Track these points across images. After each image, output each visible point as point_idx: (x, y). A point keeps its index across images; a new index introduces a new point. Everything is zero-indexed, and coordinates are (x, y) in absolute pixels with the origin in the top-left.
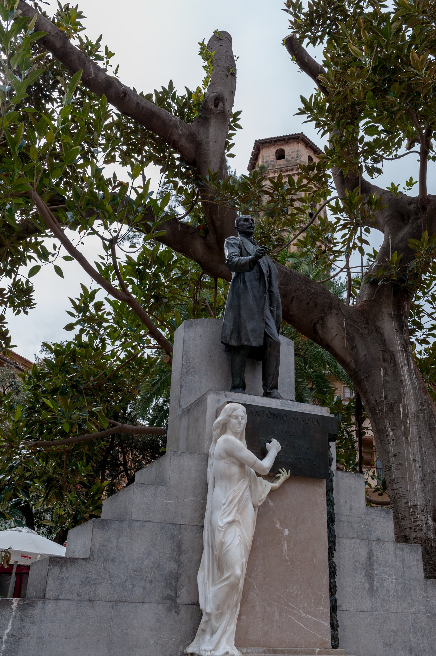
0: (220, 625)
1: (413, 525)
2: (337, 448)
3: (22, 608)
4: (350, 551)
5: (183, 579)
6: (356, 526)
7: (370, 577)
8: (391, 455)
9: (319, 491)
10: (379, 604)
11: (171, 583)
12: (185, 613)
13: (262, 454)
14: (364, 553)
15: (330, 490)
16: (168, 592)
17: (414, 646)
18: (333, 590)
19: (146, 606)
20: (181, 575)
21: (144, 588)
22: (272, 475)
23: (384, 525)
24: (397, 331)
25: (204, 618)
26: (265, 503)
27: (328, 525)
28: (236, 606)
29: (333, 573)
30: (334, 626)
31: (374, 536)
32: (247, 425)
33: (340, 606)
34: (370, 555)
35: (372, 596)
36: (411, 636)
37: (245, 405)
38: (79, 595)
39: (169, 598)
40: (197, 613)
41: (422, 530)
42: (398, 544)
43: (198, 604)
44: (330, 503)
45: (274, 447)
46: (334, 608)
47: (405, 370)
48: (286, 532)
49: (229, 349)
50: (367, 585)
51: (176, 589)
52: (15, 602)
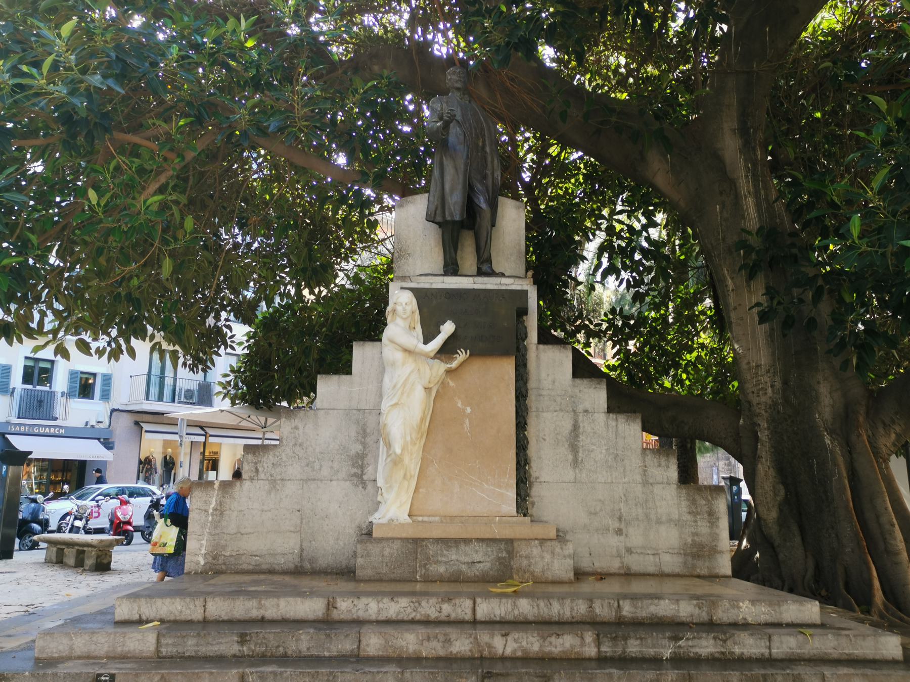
1: (755, 389)
4: (546, 426)
6: (559, 399)
7: (574, 448)
8: (731, 308)
9: (507, 367)
10: (584, 475)
11: (357, 462)
14: (566, 425)
16: (355, 470)
17: (624, 514)
19: (334, 483)
20: (367, 455)
21: (332, 467)
31: (581, 408)
33: (537, 478)
34: (576, 427)
35: (575, 468)
36: (622, 505)
38: (271, 476)
39: (355, 475)
41: (766, 393)
42: (611, 415)
47: (750, 201)
50: (570, 457)
51: (362, 467)
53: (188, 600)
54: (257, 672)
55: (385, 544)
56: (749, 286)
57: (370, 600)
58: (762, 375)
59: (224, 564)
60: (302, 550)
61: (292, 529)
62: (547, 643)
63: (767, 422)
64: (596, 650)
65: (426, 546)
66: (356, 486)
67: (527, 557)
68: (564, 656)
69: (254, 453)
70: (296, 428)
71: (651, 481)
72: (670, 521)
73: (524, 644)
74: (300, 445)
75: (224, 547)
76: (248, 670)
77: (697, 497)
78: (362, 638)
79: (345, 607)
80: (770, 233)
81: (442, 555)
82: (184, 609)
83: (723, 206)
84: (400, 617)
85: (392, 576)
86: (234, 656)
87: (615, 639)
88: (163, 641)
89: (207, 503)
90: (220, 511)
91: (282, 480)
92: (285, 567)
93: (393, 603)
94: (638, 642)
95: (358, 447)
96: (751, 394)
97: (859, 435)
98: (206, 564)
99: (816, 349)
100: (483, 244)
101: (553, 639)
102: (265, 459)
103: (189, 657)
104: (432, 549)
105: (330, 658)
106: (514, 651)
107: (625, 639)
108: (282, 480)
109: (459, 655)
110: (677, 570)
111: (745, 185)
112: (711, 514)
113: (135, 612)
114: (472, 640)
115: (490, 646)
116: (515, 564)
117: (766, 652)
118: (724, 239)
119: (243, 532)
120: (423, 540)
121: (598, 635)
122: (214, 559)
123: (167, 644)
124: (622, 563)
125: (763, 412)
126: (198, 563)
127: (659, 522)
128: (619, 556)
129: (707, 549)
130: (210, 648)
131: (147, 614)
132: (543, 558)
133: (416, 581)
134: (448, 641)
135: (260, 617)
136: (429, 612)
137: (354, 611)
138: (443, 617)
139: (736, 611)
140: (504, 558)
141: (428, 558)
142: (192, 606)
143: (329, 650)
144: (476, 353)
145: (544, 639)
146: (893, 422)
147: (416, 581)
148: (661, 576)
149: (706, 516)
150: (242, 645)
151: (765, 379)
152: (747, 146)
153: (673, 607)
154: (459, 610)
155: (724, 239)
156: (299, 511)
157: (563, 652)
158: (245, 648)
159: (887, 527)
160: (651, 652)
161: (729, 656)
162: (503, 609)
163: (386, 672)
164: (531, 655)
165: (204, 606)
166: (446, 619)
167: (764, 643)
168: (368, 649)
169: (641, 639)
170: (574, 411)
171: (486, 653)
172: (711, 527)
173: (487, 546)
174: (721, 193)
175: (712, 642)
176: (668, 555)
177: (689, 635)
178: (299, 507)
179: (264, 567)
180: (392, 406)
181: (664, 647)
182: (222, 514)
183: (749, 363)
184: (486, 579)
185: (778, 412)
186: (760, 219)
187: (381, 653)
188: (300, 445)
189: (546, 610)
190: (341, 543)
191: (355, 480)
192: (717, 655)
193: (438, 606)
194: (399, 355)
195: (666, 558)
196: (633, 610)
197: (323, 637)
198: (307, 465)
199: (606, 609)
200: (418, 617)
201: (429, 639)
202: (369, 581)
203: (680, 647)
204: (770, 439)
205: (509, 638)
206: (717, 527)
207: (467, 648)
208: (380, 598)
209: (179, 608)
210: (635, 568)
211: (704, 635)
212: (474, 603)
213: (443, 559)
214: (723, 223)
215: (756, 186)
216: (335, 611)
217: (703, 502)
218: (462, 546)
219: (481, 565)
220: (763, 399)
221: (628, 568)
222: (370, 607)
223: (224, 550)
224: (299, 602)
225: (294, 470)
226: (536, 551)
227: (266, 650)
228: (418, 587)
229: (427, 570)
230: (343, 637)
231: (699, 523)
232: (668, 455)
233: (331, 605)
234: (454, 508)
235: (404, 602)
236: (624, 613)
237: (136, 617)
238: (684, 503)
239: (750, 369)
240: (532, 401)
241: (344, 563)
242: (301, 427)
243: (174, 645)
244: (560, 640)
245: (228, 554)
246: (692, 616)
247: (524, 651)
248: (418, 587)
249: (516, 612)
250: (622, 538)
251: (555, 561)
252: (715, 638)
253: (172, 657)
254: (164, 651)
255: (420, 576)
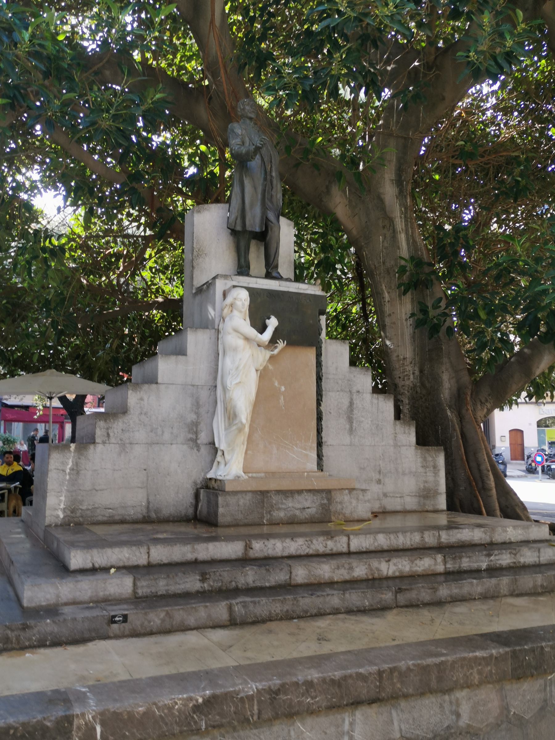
0: (232, 457)
2: (327, 320)
3: (78, 450)
4: (333, 400)
5: (203, 426)
6: (340, 382)
7: (350, 420)
9: (310, 354)
11: (192, 429)
12: (204, 450)
13: (262, 329)
14: (346, 402)
15: (319, 355)
16: (191, 436)
18: (319, 431)
20: (200, 423)
21: (172, 433)
22: (273, 341)
23: (364, 380)
24: (397, 198)
25: (219, 453)
26: (265, 368)
27: (317, 382)
28: (243, 444)
29: (319, 418)
30: (320, 456)
31: (354, 389)
32: (250, 306)
33: (326, 442)
34: (351, 404)
36: (381, 462)
37: (248, 289)
38: (121, 440)
39: (191, 439)
40: (215, 450)
42: (374, 395)
43: (214, 443)
44: (319, 364)
45: (273, 323)
46: (320, 444)
48: (283, 389)
49: (234, 232)
50: (348, 426)
51: (196, 433)
52: (73, 446)
53: (134, 548)
54: (241, 602)
55: (240, 496)
56: (400, 299)
57: (277, 541)
58: (407, 366)
59: (82, 517)
60: (149, 503)
61: (140, 485)
62: (414, 565)
63: (409, 399)
64: (443, 567)
65: (271, 497)
66: (192, 448)
67: (341, 503)
68: (424, 573)
69: (105, 421)
70: (142, 399)
71: (399, 444)
72: (410, 472)
73: (400, 566)
74: (146, 414)
75: (81, 502)
76: (234, 602)
77: (427, 455)
78: (292, 571)
79: (259, 548)
80: (417, 261)
81: (282, 503)
82: (131, 556)
83: (385, 237)
84: (298, 553)
85: (246, 521)
86: (198, 592)
87: (454, 559)
88: (139, 584)
89: (64, 464)
90: (76, 470)
91: (131, 444)
92: (135, 517)
93: (293, 543)
94: (468, 559)
95: (193, 417)
96: (398, 379)
97: (467, 410)
98: (64, 517)
99: (442, 349)
100: (272, 252)
101: (418, 562)
102: (115, 425)
103: (161, 595)
104: (275, 499)
105: (270, 588)
106: (394, 572)
107: (461, 558)
108: (131, 444)
109: (359, 578)
110: (414, 508)
111: (400, 224)
112: (435, 467)
113: (88, 561)
114: (366, 566)
115: (378, 570)
116: (332, 508)
117: (536, 559)
118: (384, 263)
119: (97, 488)
120: (268, 492)
121: (444, 557)
122: (72, 512)
123: (142, 587)
124: (381, 504)
125: (406, 392)
126: (58, 517)
127: (404, 474)
128: (379, 499)
129: (432, 492)
130: (178, 586)
131: (99, 562)
132: (351, 503)
133: (264, 525)
134: (351, 569)
135: (194, 559)
136: (318, 548)
137: (265, 550)
138: (328, 551)
139: (504, 534)
140: (325, 504)
141: (272, 506)
142: (138, 554)
143: (269, 581)
144: (291, 343)
145: (412, 562)
146: (487, 401)
147: (264, 525)
148: (405, 512)
149: (432, 469)
150: (203, 583)
151: (409, 368)
152: (401, 194)
153: (470, 534)
154: (339, 545)
155: (384, 263)
156: (145, 470)
157: (424, 570)
158: (206, 585)
159: (485, 472)
160: (475, 566)
161: (518, 565)
162: (367, 542)
163: (333, 595)
164: (405, 574)
165: (148, 553)
166: (330, 552)
167: (536, 554)
168: (297, 578)
169: (470, 557)
170: (350, 391)
171: (376, 575)
172: (435, 476)
173: (314, 495)
174: (384, 227)
175: (509, 556)
176: (409, 497)
177: (496, 552)
178: (145, 467)
179: (117, 518)
180: (237, 384)
181: (482, 561)
182: (78, 473)
183: (398, 356)
184: (311, 521)
185: (417, 392)
186: (409, 251)
187: (306, 581)
188: (145, 414)
189: (395, 541)
190: (180, 496)
191: (191, 443)
192: (511, 565)
193: (324, 543)
194: (241, 342)
195: (408, 499)
196: (447, 537)
197: (264, 572)
198: (151, 431)
199: (432, 539)
200: (311, 552)
201: (338, 568)
202: (229, 526)
203: (491, 561)
204: (409, 411)
205: (391, 563)
206: (439, 476)
207: (364, 572)
208: (283, 540)
209: (127, 555)
210: (389, 508)
211: (504, 551)
212: (349, 539)
213: (283, 506)
214: (384, 250)
215: (406, 225)
216: (251, 551)
217: (431, 459)
218: (296, 496)
219: (310, 510)
220: (407, 383)
221: (385, 508)
222: (277, 547)
223: (81, 504)
224: (224, 546)
225: (140, 435)
226: (346, 498)
227: (222, 585)
228: (265, 530)
229: (271, 515)
230: (278, 571)
231: (428, 474)
232: (409, 426)
233: (248, 547)
234: (273, 466)
235: (301, 541)
236: (442, 540)
237: (90, 565)
238: (419, 460)
239: (399, 361)
240: (324, 385)
241: (183, 513)
242: (146, 398)
243: (148, 586)
244: (422, 562)
245: (84, 508)
246: (481, 539)
247: (400, 571)
248: (265, 530)
249: (376, 544)
250: (381, 486)
251: (359, 505)
252: (510, 553)
253: (147, 597)
254: (140, 592)
255: (267, 521)
